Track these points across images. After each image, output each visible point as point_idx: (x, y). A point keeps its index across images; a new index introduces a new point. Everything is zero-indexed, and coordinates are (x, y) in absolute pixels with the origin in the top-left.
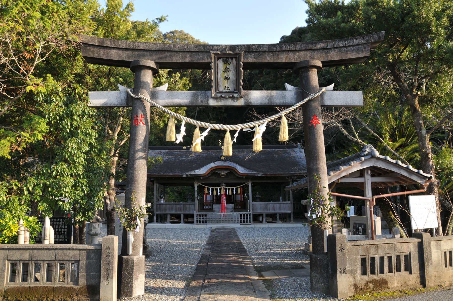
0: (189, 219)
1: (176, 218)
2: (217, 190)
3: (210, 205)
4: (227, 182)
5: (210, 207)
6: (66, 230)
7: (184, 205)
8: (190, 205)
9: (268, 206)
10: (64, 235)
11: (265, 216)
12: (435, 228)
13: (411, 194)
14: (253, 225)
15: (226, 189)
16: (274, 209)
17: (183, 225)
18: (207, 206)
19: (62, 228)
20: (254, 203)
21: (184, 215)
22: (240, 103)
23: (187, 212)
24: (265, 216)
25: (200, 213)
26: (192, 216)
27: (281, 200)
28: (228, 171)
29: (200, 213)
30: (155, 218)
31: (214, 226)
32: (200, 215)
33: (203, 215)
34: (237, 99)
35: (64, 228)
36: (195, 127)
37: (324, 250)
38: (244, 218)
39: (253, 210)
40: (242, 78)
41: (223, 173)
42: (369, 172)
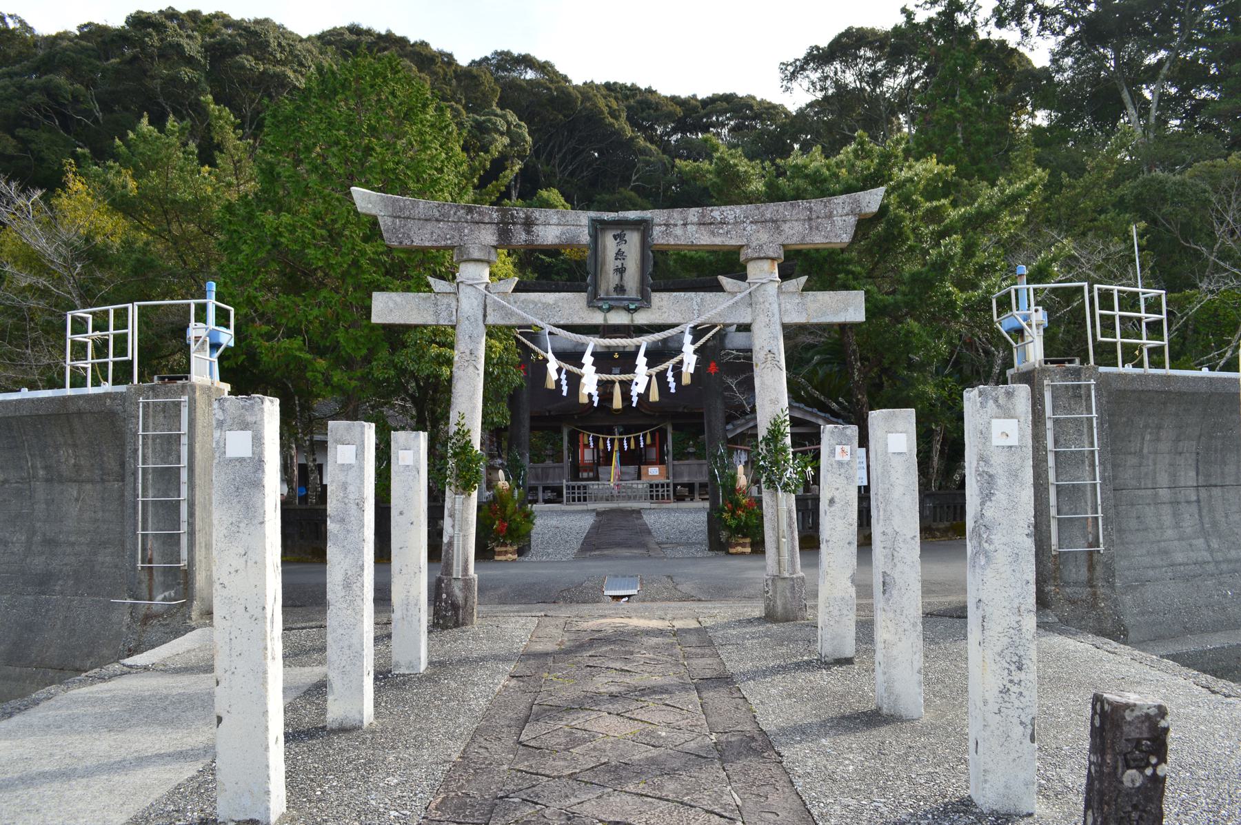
2: (605, 440)
3: (591, 470)
6: (815, 812)
11: (697, 486)
14: (674, 505)
15: (621, 441)
23: (550, 482)
24: (540, 489)
25: (573, 483)
27: (1167, 365)
32: (573, 488)
33: (579, 488)
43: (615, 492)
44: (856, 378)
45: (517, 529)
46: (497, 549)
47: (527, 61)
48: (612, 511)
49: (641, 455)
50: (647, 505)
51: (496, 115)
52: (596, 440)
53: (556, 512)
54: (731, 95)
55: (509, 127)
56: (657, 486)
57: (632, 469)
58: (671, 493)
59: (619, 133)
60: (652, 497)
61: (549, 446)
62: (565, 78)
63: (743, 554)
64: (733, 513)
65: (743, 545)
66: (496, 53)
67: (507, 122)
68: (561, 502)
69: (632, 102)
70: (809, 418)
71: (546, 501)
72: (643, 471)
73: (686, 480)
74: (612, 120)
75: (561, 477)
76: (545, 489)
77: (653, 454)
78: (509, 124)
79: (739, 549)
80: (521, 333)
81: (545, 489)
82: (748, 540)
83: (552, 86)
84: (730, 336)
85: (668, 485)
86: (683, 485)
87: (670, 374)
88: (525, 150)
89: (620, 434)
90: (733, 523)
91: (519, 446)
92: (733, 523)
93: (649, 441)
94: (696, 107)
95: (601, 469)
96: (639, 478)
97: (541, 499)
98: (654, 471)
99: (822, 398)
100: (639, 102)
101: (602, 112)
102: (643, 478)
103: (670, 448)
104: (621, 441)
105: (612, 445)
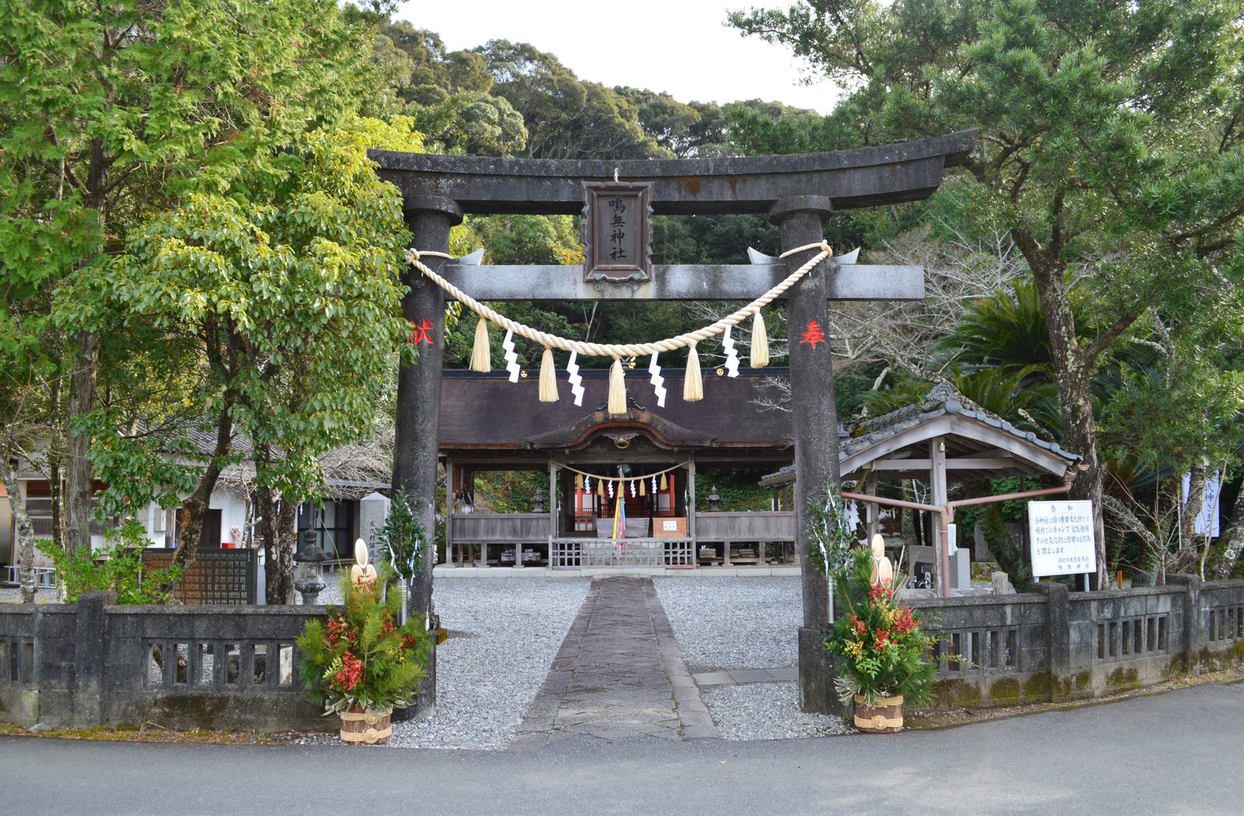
0: (539, 554)
1: (498, 554)
2: (606, 483)
3: (590, 521)
4: (633, 461)
5: (590, 526)
6: (243, 579)
7: (522, 519)
8: (538, 519)
9: (738, 521)
10: (240, 591)
11: (727, 546)
13: (1035, 498)
15: (627, 484)
16: (751, 530)
17: (483, 570)
18: (583, 521)
19: (234, 576)
20: (699, 514)
22: (647, 292)
23: (532, 539)
24: (519, 547)
26: (542, 549)
28: (633, 435)
31: (600, 572)
32: (562, 547)
33: (570, 546)
34: (641, 282)
35: (240, 576)
36: (540, 348)
37: (827, 619)
39: (697, 532)
40: (651, 240)
41: (621, 440)
42: (943, 447)
43: (618, 554)
44: (1071, 367)
45: (387, 673)
46: (345, 716)
47: (526, 52)
48: (614, 580)
49: (652, 503)
50: (661, 571)
51: (487, 102)
52: (594, 484)
54: (756, 100)
55: (502, 119)
56: (675, 545)
57: (642, 522)
58: (694, 555)
59: (629, 135)
60: (667, 559)
61: (539, 491)
63: (888, 731)
64: (868, 642)
65: (888, 713)
66: (491, 42)
67: (500, 110)
68: (545, 565)
69: (644, 106)
71: (527, 564)
73: (712, 538)
74: (623, 120)
75: (546, 532)
76: (525, 547)
77: (667, 502)
78: (501, 112)
79: (881, 722)
80: (423, 259)
81: (525, 547)
82: (899, 701)
83: (555, 78)
85: (689, 544)
88: (520, 146)
89: (627, 475)
90: (871, 666)
91: (411, 487)
92: (871, 666)
93: (664, 486)
94: (717, 112)
95: (601, 522)
96: (651, 534)
97: (519, 561)
98: (670, 525)
100: (654, 106)
101: (611, 111)
102: (656, 533)
103: (693, 496)
104: (627, 484)
105: (615, 490)
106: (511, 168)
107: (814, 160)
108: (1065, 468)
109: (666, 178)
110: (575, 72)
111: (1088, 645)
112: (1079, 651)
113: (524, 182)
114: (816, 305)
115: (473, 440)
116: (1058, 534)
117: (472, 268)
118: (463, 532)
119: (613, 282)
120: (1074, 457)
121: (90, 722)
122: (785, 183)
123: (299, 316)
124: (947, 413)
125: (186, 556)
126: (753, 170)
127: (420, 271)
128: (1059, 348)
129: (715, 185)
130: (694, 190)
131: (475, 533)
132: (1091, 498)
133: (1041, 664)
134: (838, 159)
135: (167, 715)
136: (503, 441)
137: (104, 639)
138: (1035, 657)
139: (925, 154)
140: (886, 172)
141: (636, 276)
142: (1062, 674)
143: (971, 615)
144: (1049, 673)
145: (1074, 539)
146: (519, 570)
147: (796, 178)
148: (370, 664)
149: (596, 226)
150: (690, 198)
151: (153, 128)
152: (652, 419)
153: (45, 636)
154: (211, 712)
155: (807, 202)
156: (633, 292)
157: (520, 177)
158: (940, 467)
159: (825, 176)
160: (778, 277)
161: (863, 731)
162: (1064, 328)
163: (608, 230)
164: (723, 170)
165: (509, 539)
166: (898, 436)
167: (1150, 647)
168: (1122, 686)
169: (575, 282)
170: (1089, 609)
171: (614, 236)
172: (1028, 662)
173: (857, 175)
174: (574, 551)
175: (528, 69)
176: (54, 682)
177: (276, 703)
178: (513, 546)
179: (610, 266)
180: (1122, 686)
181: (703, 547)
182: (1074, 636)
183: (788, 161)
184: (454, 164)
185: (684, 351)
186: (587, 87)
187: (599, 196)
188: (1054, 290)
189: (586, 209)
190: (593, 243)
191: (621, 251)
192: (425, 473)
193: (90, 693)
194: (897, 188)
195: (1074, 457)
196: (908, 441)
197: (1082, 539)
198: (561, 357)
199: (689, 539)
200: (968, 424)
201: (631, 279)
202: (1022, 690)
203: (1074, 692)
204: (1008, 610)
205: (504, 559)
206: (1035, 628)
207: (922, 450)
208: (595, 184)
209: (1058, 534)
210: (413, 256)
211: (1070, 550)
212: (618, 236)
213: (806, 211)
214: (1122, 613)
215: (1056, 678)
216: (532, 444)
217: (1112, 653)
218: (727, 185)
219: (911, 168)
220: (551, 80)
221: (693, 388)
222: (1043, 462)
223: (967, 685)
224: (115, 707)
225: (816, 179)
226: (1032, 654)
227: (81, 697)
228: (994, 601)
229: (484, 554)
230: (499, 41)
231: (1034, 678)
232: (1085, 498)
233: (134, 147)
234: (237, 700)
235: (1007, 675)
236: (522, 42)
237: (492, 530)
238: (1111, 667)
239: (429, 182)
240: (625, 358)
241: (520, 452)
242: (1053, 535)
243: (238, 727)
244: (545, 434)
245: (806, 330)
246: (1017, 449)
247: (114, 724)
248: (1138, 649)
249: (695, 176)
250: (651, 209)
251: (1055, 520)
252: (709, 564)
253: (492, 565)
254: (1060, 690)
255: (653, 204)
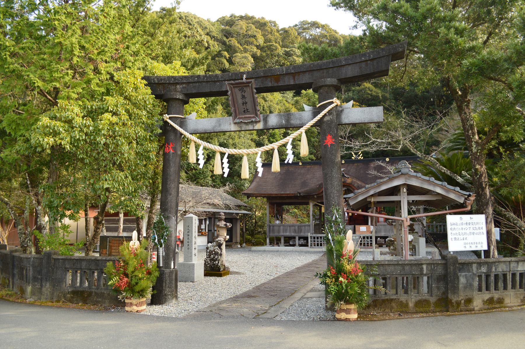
12: (484, 251)
13: (450, 214)
17: (282, 248)
21: (285, 237)
23: (302, 234)
24: (297, 238)
26: (306, 238)
29: (314, 235)
30: (268, 241)
32: (314, 238)
33: (318, 238)
34: (256, 122)
38: (314, 241)
42: (405, 190)
44: (474, 150)
47: (315, 25)
53: (298, 252)
60: (361, 244)
62: (335, 32)
65: (348, 311)
68: (307, 246)
70: (426, 186)
71: (301, 245)
72: (357, 229)
76: (300, 238)
79: (343, 315)
80: (170, 118)
82: (352, 307)
83: (328, 35)
84: (346, 111)
86: (381, 237)
87: (289, 147)
99: (448, 173)
102: (357, 233)
106: (204, 78)
107: (330, 63)
108: (463, 199)
109: (266, 77)
110: (338, 31)
111: (471, 285)
112: (465, 288)
113: (209, 83)
114: (330, 127)
115: (275, 193)
116: (464, 231)
117: (191, 121)
118: (273, 231)
119: (245, 123)
120: (468, 193)
121: (46, 299)
122: (317, 74)
123: (94, 144)
124: (402, 174)
125: (95, 238)
126: (302, 70)
127: (169, 123)
128: (469, 141)
129: (286, 78)
130: (277, 81)
131: (279, 232)
132: (485, 213)
133: (444, 293)
134: (341, 61)
135: (72, 297)
136: (288, 193)
137: (52, 268)
138: (447, 288)
139: (381, 55)
140: (363, 65)
141: (254, 120)
142: (454, 299)
143: (404, 269)
144: (447, 297)
145: (473, 233)
146: (297, 248)
147: (321, 71)
148: (131, 280)
149: (235, 100)
150: (276, 85)
151: (47, 76)
152: (352, 181)
153: (34, 266)
154: (87, 297)
155: (325, 82)
156: (254, 126)
157: (207, 82)
158: (404, 199)
159: (335, 69)
160: (315, 115)
161: (340, 320)
162: (470, 131)
163: (240, 101)
164: (289, 71)
165: (293, 234)
166: (379, 185)
167: (513, 287)
168: (493, 306)
169: (230, 124)
170: (472, 267)
171: (243, 103)
172: (435, 291)
173: (350, 68)
174: (319, 240)
175: (317, 32)
176: (36, 283)
177: (109, 294)
178: (294, 238)
179: (243, 116)
180: (493, 306)
181: (379, 239)
182: (462, 280)
183: (318, 64)
184: (182, 79)
185: (273, 150)
186: (343, 37)
187: (234, 87)
188: (465, 113)
189: (229, 93)
190: (235, 107)
191: (247, 110)
192: (171, 205)
193: (47, 288)
194: (368, 72)
195: (468, 193)
196: (384, 187)
197: (479, 234)
198: (222, 154)
199: (371, 235)
200: (414, 179)
201: (252, 121)
202: (432, 305)
203: (462, 307)
204: (425, 267)
205: (291, 243)
206: (440, 276)
207: (395, 191)
208: (230, 82)
209: (464, 231)
210: (166, 117)
211: (471, 239)
212: (245, 103)
213: (326, 86)
214: (494, 270)
215: (451, 300)
216: (300, 194)
217: (488, 289)
218: (291, 77)
219: (375, 61)
220: (326, 36)
221: (276, 166)
222: (452, 196)
223: (401, 302)
224: (55, 294)
225: (331, 71)
226: (438, 288)
227: (44, 289)
228: (416, 262)
229: (282, 241)
230: (304, 21)
231: (439, 300)
232: (482, 213)
233: (39, 85)
234: (95, 293)
235: (424, 298)
236: (314, 20)
237: (285, 231)
238: (487, 296)
239: (173, 87)
240: (248, 155)
241: (295, 197)
242: (461, 231)
243: (95, 303)
244: (306, 189)
245: (326, 139)
246: (439, 190)
247: (55, 300)
248: (505, 288)
249: (277, 75)
250: (255, 91)
251: (462, 224)
252: (382, 246)
253: (286, 246)
254: (453, 306)
255: (256, 89)
